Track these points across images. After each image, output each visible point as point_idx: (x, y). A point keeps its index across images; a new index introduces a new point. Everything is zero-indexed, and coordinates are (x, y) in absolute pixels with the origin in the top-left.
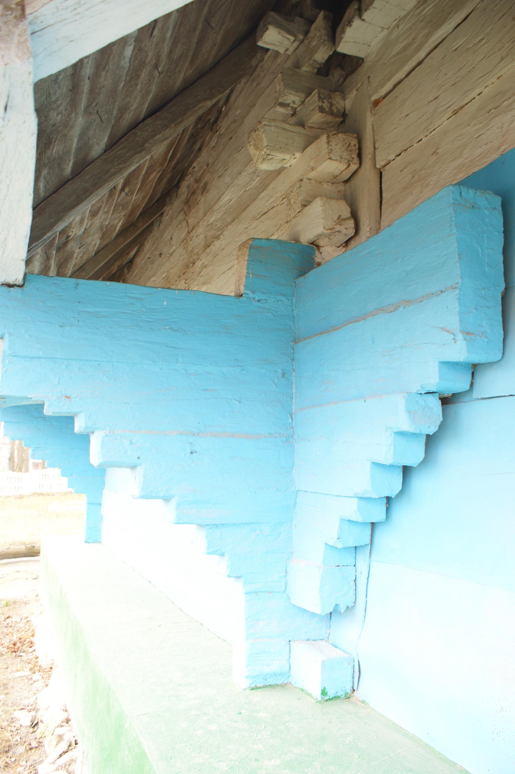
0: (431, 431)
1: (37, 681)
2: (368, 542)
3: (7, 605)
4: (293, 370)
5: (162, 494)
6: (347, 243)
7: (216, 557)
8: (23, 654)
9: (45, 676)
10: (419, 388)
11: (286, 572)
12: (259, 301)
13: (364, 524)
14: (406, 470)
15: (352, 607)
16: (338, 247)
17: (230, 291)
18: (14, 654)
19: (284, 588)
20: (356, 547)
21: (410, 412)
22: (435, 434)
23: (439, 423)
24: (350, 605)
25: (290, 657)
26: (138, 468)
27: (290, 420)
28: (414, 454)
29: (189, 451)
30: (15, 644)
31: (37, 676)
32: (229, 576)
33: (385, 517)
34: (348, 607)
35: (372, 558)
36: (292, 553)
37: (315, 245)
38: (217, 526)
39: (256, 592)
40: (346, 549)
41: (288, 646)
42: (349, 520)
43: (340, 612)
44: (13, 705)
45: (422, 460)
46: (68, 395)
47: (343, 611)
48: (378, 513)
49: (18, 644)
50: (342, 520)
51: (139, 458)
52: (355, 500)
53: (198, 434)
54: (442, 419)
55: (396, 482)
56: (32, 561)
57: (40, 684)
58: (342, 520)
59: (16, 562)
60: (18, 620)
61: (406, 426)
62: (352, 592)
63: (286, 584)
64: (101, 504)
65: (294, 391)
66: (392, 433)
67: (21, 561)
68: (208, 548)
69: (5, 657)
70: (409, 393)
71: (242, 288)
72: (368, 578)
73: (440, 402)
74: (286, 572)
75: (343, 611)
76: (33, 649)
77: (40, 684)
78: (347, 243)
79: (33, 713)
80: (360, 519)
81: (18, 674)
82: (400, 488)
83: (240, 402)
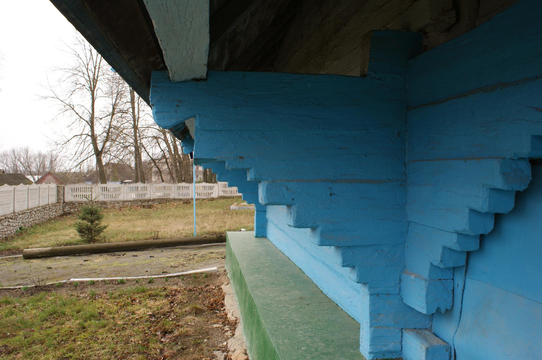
0: (522, 188)
1: (227, 331)
2: (463, 262)
3: (206, 277)
4: (406, 131)
5: (310, 225)
6: (449, 29)
7: (348, 269)
8: (218, 312)
9: (233, 328)
10: (513, 155)
11: (400, 280)
12: (379, 79)
13: (462, 252)
14: (498, 218)
15: (450, 310)
16: (442, 32)
17: (357, 73)
18: (212, 311)
19: (398, 291)
20: (454, 268)
21: (504, 174)
22: (525, 191)
23: (528, 182)
24: (449, 308)
25: (402, 340)
26: (293, 207)
27: (404, 169)
28: (507, 205)
29: (329, 193)
30: (212, 305)
31: (227, 328)
32: (358, 282)
33: (478, 247)
34: (447, 310)
35: (467, 276)
36: (405, 267)
37: (423, 32)
38: (350, 247)
39: (378, 294)
40: (448, 269)
41: (401, 333)
42: (449, 249)
43: (441, 313)
44: (213, 346)
45: (512, 209)
46: (242, 156)
47: (443, 312)
48: (474, 245)
49: (214, 305)
50: (445, 248)
51: (293, 199)
52: (455, 236)
53: (336, 181)
54: (531, 178)
55: (489, 225)
56: (221, 245)
57: (229, 334)
58: (445, 248)
59: (211, 246)
60: (214, 287)
61: (499, 184)
62: (450, 299)
63: (400, 289)
64: (266, 211)
65: (407, 146)
66: (488, 189)
67: (214, 245)
68: (343, 262)
69: (206, 313)
70: (504, 159)
71: (366, 69)
72: (463, 290)
73: (530, 165)
74: (400, 280)
75: (443, 312)
76: (224, 308)
77: (229, 334)
78: (449, 29)
79: (225, 353)
80: (459, 249)
81: (215, 326)
82: (492, 228)
83: (366, 156)
